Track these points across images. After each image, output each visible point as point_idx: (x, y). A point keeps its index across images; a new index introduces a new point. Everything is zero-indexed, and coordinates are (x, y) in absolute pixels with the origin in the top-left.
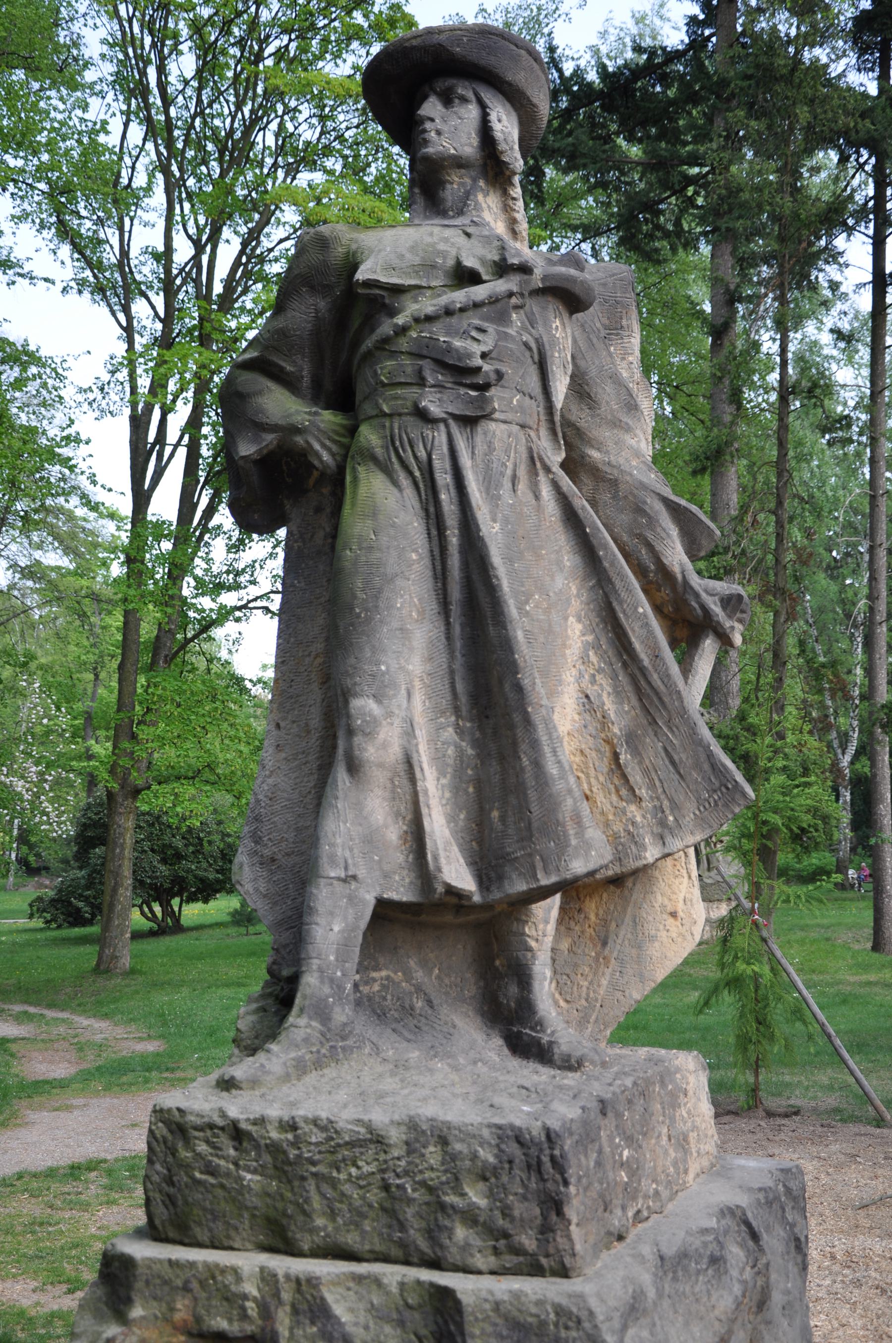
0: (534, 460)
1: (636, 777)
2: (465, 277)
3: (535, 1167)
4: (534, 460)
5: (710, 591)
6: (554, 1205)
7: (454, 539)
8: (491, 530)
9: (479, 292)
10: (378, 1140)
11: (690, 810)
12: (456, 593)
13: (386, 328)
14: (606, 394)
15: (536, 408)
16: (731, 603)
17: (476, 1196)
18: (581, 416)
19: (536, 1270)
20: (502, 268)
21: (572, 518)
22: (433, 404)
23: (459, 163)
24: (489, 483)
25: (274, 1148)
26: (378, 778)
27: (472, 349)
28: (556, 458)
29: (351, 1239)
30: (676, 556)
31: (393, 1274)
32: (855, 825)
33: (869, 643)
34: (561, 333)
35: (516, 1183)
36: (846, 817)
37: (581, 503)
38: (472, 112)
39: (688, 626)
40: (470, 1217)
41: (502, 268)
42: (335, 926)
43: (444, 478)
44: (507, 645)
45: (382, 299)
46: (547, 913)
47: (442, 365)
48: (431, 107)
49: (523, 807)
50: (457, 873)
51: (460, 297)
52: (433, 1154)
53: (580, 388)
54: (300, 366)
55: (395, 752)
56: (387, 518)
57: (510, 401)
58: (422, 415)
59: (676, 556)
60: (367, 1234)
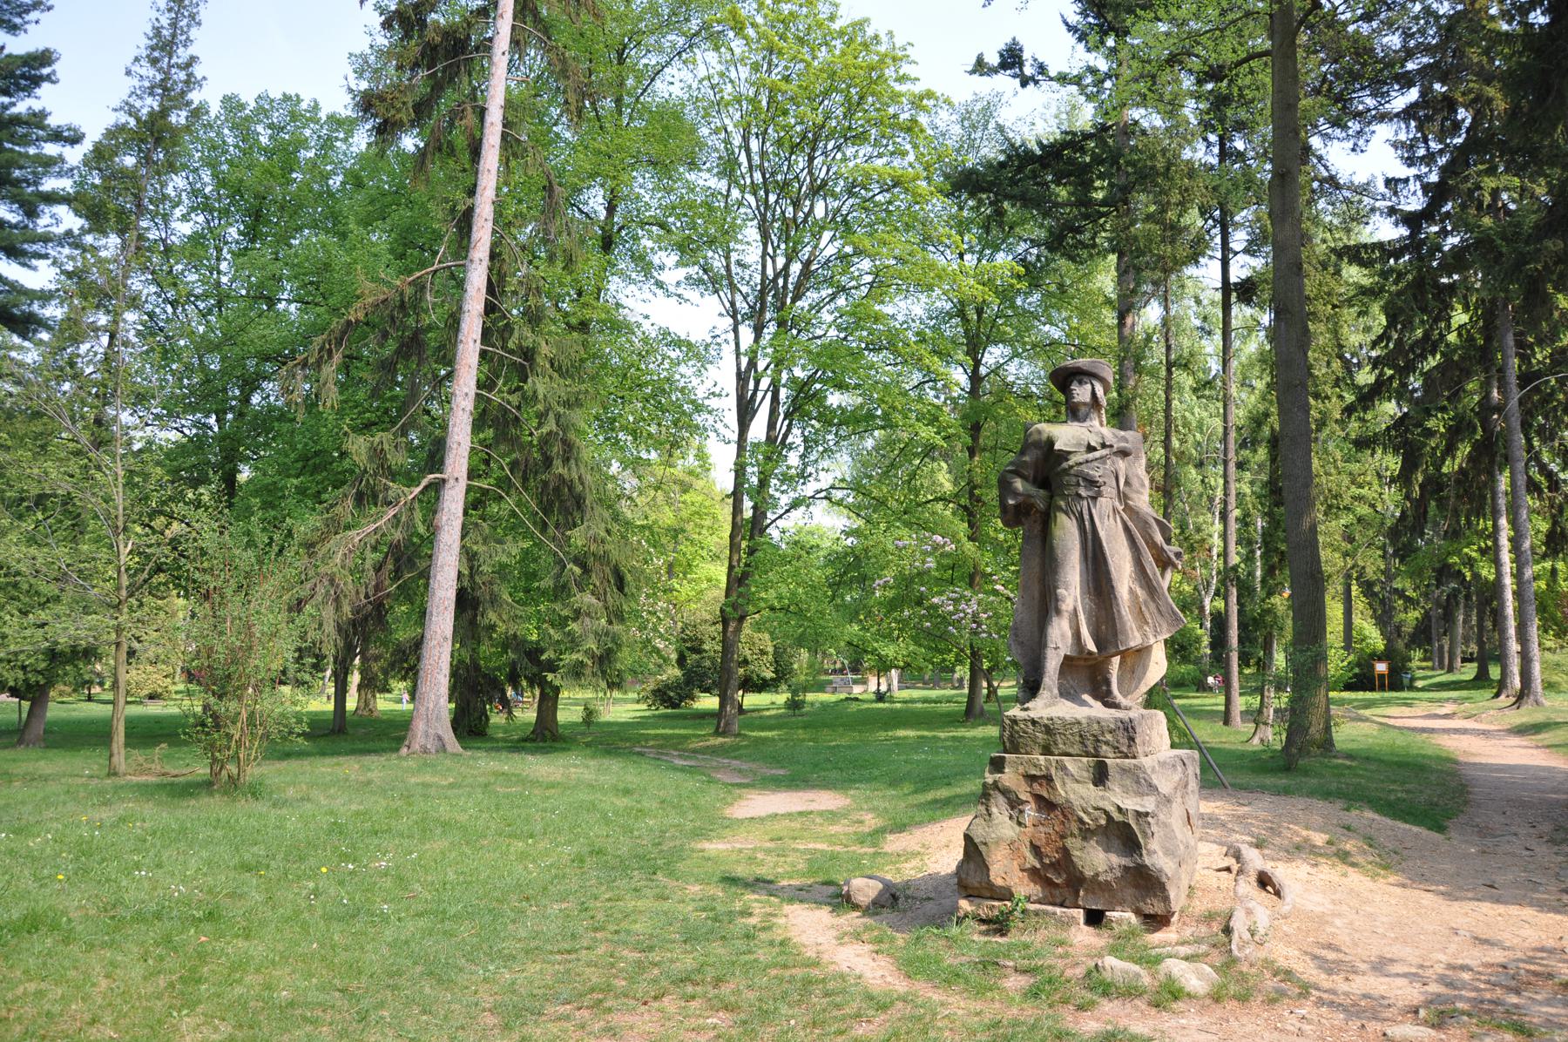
0: (1115, 510)
1: (1147, 616)
2: (1090, 449)
3: (1126, 729)
4: (1115, 510)
5: (1171, 550)
6: (1132, 739)
7: (1090, 537)
8: (1102, 534)
9: (1097, 454)
10: (1079, 723)
11: (1165, 626)
12: (1090, 555)
13: (1065, 465)
14: (1135, 482)
15: (1115, 492)
16: (1178, 555)
17: (1109, 737)
18: (1127, 490)
19: (1127, 757)
20: (1104, 446)
21: (1127, 529)
22: (1083, 492)
23: (1085, 404)
24: (1101, 518)
25: (1046, 726)
26: (1066, 615)
27: (1095, 474)
28: (1121, 508)
29: (1071, 751)
30: (1159, 538)
31: (1085, 760)
32: (1213, 646)
33: (1224, 517)
34: (1121, 464)
35: (1120, 733)
36: (1206, 641)
37: (1130, 523)
38: (1089, 387)
39: (1164, 563)
40: (1107, 743)
41: (1104, 446)
42: (1053, 663)
43: (1086, 517)
44: (1108, 573)
45: (1064, 455)
46: (1116, 660)
47: (1085, 479)
48: (1075, 387)
49: (1114, 625)
50: (1091, 646)
51: (1091, 456)
52: (1096, 726)
53: (1127, 483)
54: (1030, 473)
55: (1071, 608)
56: (1067, 532)
57: (1109, 491)
58: (1079, 496)
59: (1159, 538)
60: (1075, 749)
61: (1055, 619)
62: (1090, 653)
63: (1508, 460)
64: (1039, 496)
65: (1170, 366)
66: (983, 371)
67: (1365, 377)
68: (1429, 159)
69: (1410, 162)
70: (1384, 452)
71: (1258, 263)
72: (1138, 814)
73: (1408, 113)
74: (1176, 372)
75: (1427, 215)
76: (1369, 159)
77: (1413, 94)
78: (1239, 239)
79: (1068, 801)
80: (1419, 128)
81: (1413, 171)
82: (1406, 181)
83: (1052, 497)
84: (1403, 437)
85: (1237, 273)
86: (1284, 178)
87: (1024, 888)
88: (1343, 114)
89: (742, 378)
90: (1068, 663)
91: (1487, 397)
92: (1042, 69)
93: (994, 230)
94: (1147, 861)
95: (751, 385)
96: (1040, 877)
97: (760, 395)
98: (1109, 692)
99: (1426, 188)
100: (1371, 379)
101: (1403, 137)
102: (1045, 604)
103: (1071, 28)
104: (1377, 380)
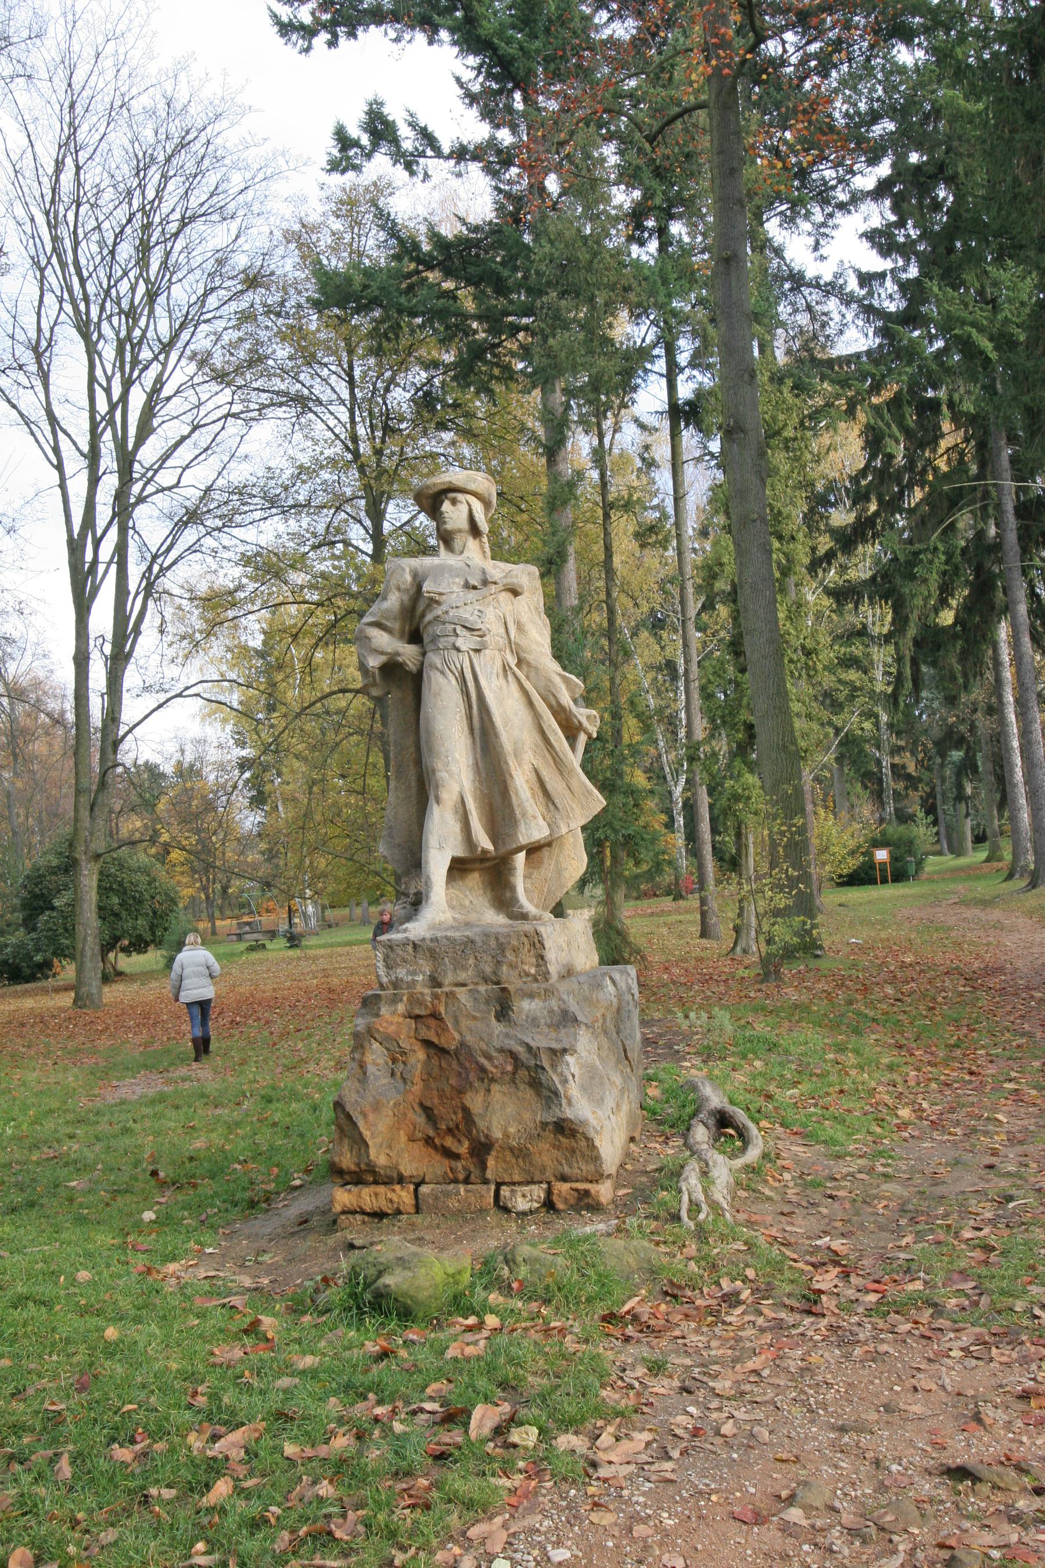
46: (521, 858)
48: (446, 506)
50: (485, 843)
61: (435, 807)
62: (484, 851)
63: (1007, 609)
64: (408, 653)
65: (608, 507)
66: (387, 527)
67: (841, 517)
68: (906, 250)
69: (885, 251)
70: (872, 603)
71: (705, 380)
72: (553, 1052)
73: (882, 189)
74: (614, 515)
75: (910, 318)
76: (837, 249)
77: (884, 169)
78: (686, 348)
79: (462, 1044)
80: (895, 208)
81: (887, 264)
82: (882, 276)
83: (424, 654)
84: (886, 585)
85: (685, 391)
86: (728, 261)
87: (412, 1161)
88: (802, 195)
89: (75, 547)
90: (458, 868)
91: (980, 534)
92: (427, 137)
93: (387, 344)
94: (569, 1113)
95: (89, 556)
96: (435, 1147)
97: (101, 568)
98: (514, 900)
99: (904, 287)
100: (850, 518)
101: (876, 222)
102: (422, 790)
103: (472, 98)
104: (858, 518)
